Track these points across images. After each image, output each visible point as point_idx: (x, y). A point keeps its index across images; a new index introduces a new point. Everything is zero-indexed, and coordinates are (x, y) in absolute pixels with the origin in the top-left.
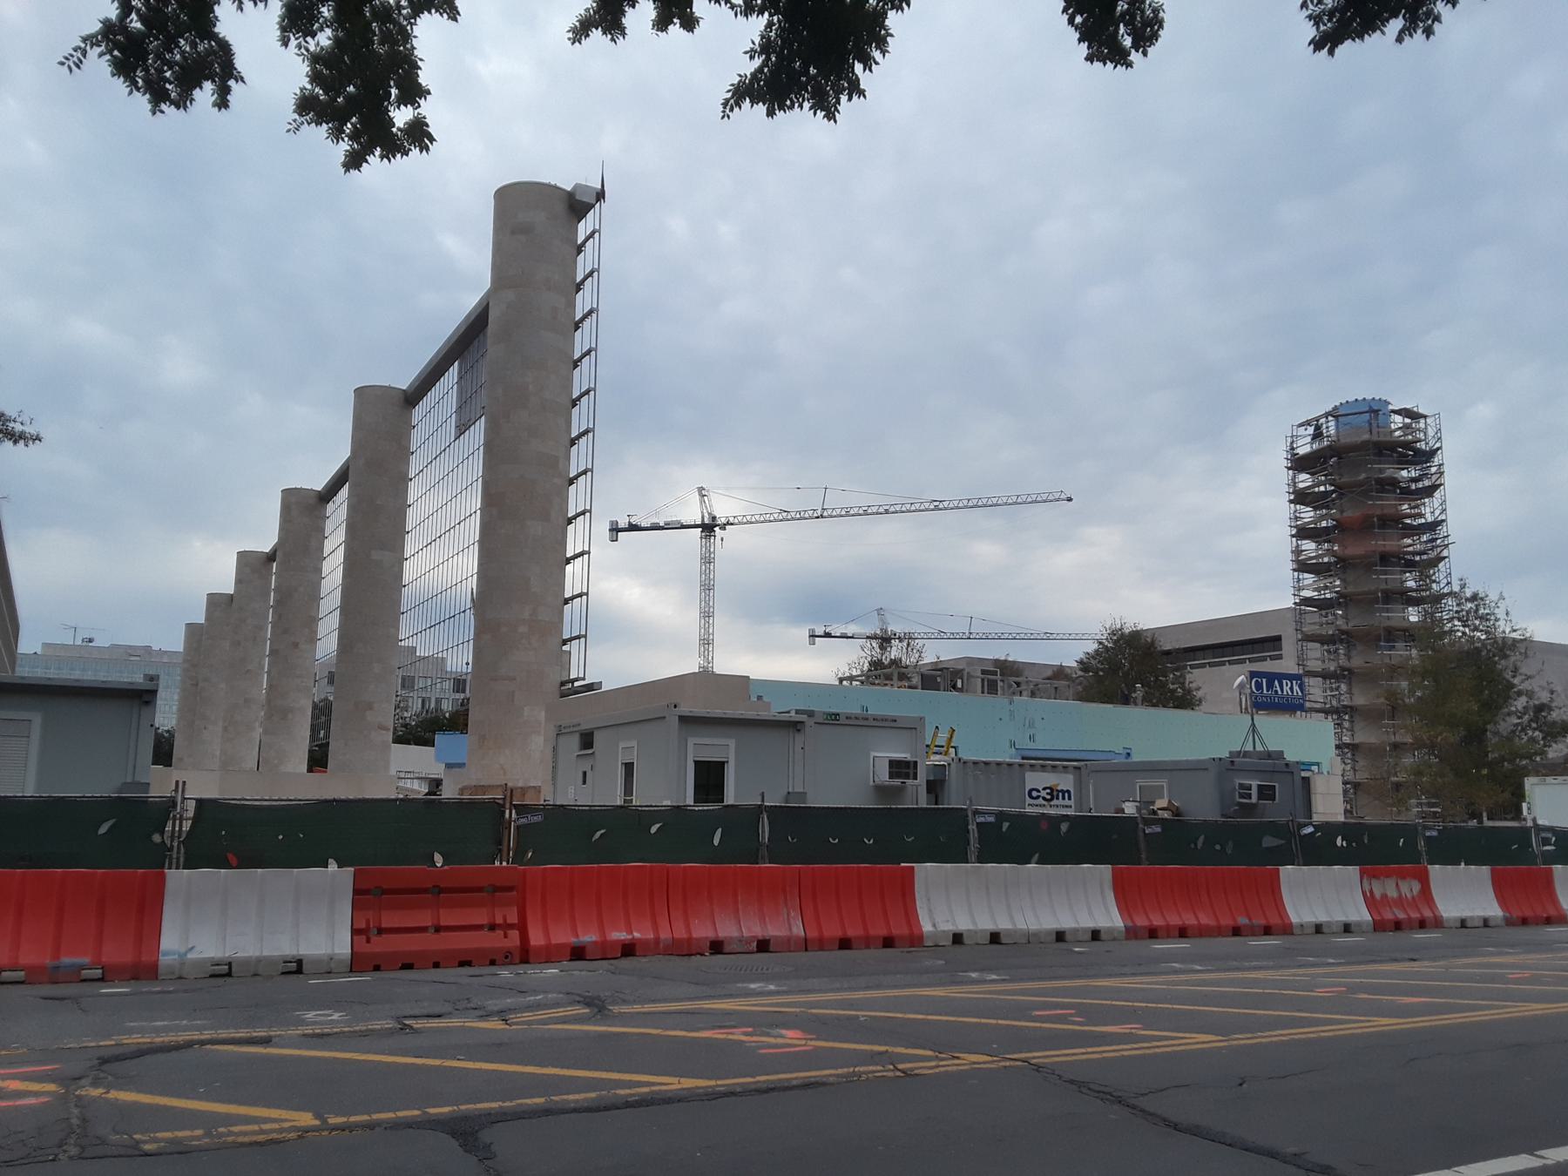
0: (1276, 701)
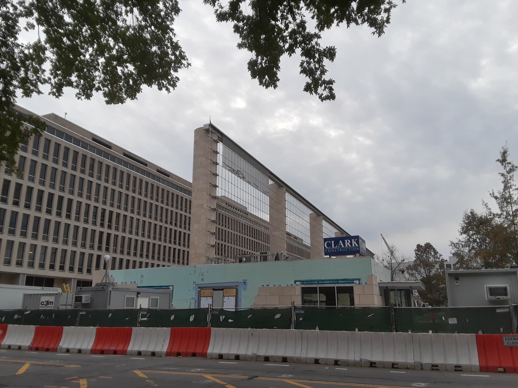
0: (340, 250)
